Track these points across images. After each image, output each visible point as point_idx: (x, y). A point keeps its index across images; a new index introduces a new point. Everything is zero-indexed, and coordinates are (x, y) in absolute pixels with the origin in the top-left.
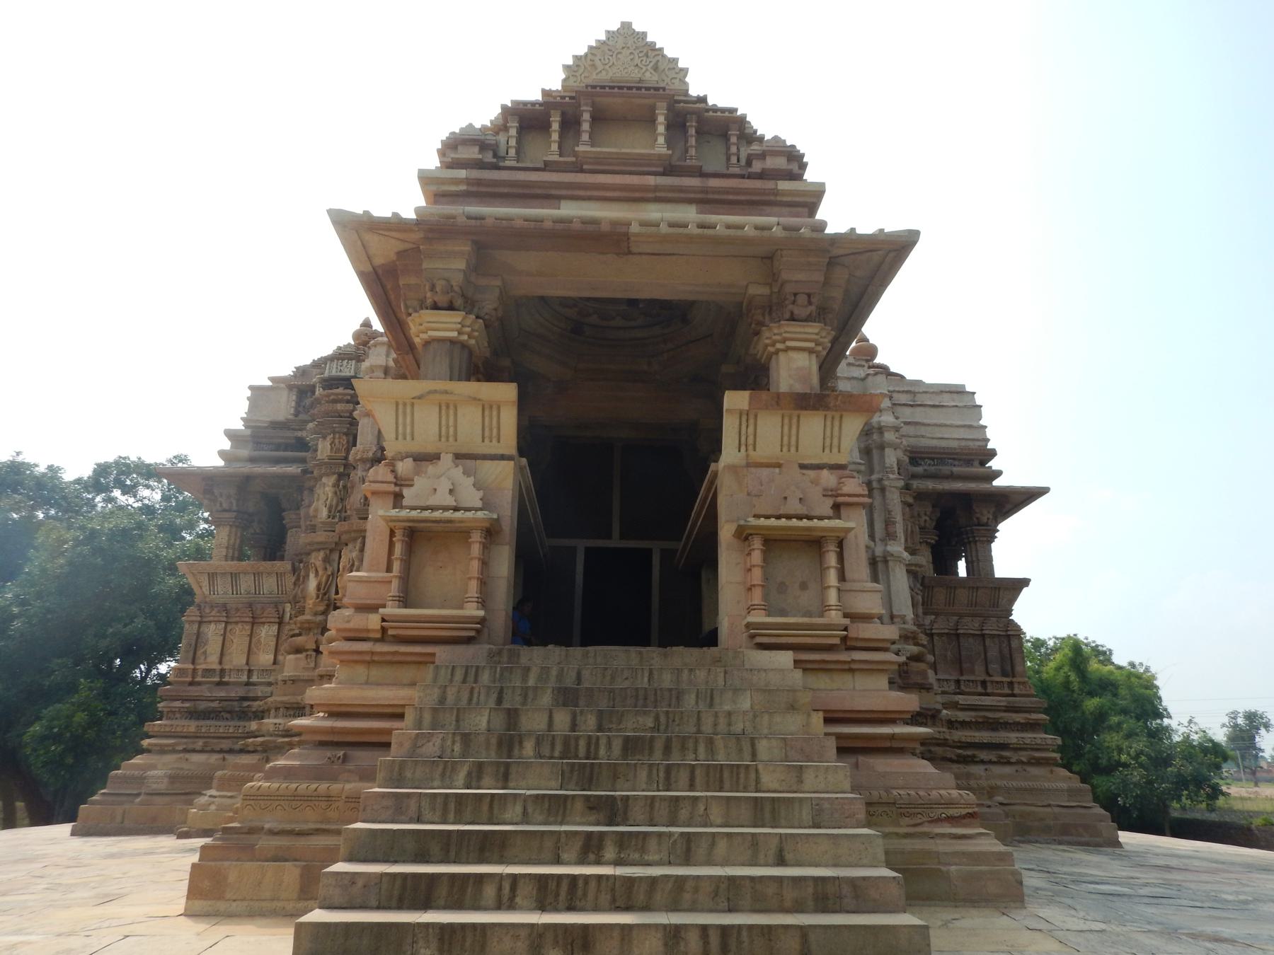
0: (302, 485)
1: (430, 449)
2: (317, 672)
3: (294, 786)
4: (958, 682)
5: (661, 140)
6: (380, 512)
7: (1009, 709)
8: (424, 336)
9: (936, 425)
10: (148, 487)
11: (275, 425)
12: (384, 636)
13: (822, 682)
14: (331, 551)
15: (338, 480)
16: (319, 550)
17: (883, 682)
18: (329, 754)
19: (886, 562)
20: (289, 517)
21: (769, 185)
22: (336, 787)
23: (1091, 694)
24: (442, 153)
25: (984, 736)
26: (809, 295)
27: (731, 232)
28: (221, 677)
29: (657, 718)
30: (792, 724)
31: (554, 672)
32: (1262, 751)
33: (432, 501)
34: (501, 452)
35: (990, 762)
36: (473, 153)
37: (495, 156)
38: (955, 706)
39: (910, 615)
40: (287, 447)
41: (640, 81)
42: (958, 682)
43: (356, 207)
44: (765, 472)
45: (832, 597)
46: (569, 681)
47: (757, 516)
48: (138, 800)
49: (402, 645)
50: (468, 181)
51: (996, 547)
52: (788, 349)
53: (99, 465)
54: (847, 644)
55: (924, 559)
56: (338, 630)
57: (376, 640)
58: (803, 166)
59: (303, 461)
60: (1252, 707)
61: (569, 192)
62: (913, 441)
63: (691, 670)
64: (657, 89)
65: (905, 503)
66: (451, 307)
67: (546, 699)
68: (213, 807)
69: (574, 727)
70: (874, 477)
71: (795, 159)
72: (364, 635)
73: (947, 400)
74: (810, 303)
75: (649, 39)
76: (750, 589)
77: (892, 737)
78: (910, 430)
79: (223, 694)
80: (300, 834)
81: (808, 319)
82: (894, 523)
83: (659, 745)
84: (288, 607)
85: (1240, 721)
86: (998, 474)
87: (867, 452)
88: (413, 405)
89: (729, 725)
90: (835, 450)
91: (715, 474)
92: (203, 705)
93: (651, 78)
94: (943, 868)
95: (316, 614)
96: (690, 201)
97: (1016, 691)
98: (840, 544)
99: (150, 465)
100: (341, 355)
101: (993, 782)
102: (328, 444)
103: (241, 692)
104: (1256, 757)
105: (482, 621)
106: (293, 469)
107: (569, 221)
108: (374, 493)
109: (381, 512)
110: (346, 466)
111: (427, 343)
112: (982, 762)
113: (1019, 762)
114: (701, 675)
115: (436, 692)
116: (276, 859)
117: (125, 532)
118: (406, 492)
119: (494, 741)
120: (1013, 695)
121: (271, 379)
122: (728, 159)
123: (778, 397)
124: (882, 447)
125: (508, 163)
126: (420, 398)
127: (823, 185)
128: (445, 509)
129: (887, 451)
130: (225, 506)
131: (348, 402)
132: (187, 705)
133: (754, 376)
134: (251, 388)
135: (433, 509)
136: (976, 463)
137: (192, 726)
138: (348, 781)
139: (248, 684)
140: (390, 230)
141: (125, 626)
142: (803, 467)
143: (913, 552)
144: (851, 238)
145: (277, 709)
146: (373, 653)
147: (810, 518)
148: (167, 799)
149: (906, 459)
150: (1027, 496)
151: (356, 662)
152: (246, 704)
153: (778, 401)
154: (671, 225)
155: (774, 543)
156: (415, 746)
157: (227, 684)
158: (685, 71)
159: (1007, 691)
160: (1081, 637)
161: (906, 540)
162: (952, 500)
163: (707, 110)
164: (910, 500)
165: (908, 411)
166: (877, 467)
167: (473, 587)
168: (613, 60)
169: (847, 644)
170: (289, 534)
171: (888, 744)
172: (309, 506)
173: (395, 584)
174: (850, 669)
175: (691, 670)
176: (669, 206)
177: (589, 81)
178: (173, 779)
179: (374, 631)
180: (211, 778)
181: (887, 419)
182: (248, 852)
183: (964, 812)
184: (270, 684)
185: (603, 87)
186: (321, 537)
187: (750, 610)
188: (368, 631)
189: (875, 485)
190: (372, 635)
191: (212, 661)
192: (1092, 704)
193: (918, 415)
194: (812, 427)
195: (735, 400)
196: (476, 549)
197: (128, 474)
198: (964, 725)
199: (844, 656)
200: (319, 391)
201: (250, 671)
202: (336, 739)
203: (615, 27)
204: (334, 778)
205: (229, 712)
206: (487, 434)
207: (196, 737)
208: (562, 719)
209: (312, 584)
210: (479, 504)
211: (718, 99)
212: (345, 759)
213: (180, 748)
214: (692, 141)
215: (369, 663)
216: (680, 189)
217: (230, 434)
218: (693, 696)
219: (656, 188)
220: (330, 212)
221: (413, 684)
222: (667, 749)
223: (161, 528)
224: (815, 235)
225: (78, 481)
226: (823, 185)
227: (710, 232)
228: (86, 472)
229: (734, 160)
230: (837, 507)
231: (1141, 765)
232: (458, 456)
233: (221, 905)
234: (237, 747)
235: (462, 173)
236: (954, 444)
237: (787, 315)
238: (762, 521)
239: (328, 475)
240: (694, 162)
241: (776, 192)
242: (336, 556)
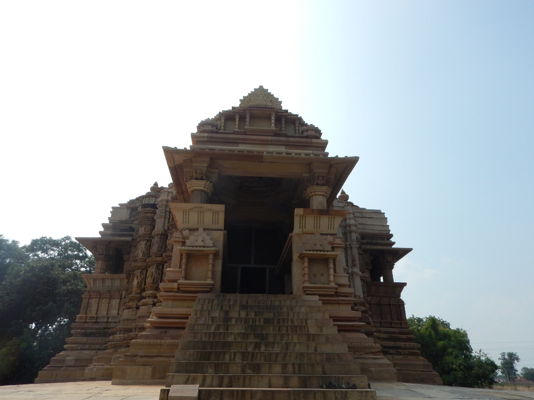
0: (130, 246)
1: (195, 227)
2: (137, 316)
3: (149, 341)
4: (381, 322)
5: (273, 125)
6: (177, 248)
8: (192, 189)
9: (371, 225)
10: (53, 250)
11: (121, 222)
13: (329, 307)
14: (143, 269)
15: (147, 243)
16: (138, 269)
17: (349, 308)
18: (160, 330)
19: (353, 275)
20: (125, 257)
21: (309, 140)
22: (163, 341)
23: (440, 340)
24: (198, 127)
25: (392, 344)
26: (323, 177)
27: (297, 156)
28: (97, 320)
29: (274, 314)
30: (319, 316)
31: (239, 301)
32: (517, 371)
34: (219, 228)
35: (394, 354)
36: (209, 128)
37: (217, 129)
39: (362, 296)
40: (125, 230)
41: (266, 105)
43: (171, 145)
44: (309, 236)
46: (244, 303)
47: (306, 250)
48: (62, 369)
49: (185, 294)
50: (208, 137)
51: (394, 271)
52: (316, 195)
53: (33, 240)
54: (337, 294)
55: (367, 275)
56: (163, 288)
57: (176, 292)
58: (321, 134)
59: (132, 235)
60: (514, 351)
61: (242, 141)
62: (362, 231)
63: (285, 301)
64: (272, 108)
65: (359, 253)
67: (237, 308)
68: (95, 369)
69: (247, 315)
70: (348, 243)
71: (317, 132)
72: (172, 290)
73: (374, 216)
74: (323, 180)
75: (269, 91)
76: (304, 276)
77: (353, 326)
78: (361, 226)
80: (152, 357)
81: (323, 185)
82: (355, 261)
83: (276, 321)
84: (124, 292)
85: (506, 357)
86: (394, 243)
87: (345, 234)
88: (189, 212)
89: (298, 316)
90: (332, 229)
91: (291, 237)
93: (270, 104)
94: (370, 369)
95: (136, 294)
96: (283, 145)
97: (403, 326)
98: (334, 260)
99: (55, 240)
100: (148, 195)
102: (143, 229)
103: (104, 325)
104: (515, 374)
105: (213, 285)
107: (242, 151)
108: (175, 242)
109: (179, 247)
110: (150, 237)
111: (193, 191)
112: (391, 354)
113: (405, 354)
114: (288, 302)
115: (200, 306)
116: (143, 365)
117: (46, 267)
118: (187, 241)
119: (222, 319)
120: (402, 328)
121: (119, 204)
122: (295, 131)
123: (313, 211)
124: (350, 232)
125: (221, 131)
126: (192, 209)
127: (327, 141)
128: (200, 247)
130: (101, 253)
131: (151, 213)
133: (305, 204)
134: (113, 208)
135: (196, 247)
136: (386, 239)
137: (84, 339)
138: (167, 340)
139: (107, 322)
140: (183, 153)
141: (44, 306)
142: (321, 234)
143: (362, 272)
144: (336, 159)
145: (120, 331)
146: (175, 296)
147: (324, 251)
148: (74, 368)
149: (359, 237)
150: (404, 252)
151: (168, 299)
152: (106, 330)
153: (313, 212)
154: (277, 153)
155: (313, 260)
156: (196, 321)
157: (99, 322)
158: (281, 102)
159: (399, 326)
160: (436, 317)
161: (360, 268)
162: (377, 251)
163: (288, 115)
164: (361, 252)
165: (360, 219)
166: (349, 240)
167: (210, 274)
168: (257, 98)
169: (337, 294)
170: (125, 263)
171: (351, 328)
172: (134, 253)
173: (183, 272)
174: (338, 303)
175: (285, 301)
176: (276, 147)
177: (249, 105)
178: (76, 360)
179: (175, 288)
180: (92, 360)
181: (352, 222)
183: (377, 350)
184: (116, 322)
185: (254, 107)
186: (139, 264)
188: (173, 288)
189: (348, 246)
190: (174, 290)
191: (93, 314)
192: (440, 344)
193: (364, 221)
194: (324, 221)
195: (298, 211)
196: (211, 261)
197: (44, 244)
199: (336, 299)
200: (140, 209)
201: (108, 318)
202: (162, 325)
203: (257, 87)
204: (162, 339)
205: (99, 334)
206: (214, 222)
207: (85, 344)
208: (243, 314)
209: (135, 282)
210: (212, 245)
211: (293, 110)
212: (166, 332)
213: (79, 348)
214: (283, 125)
215: (173, 300)
216: (280, 141)
217: (104, 225)
218: (286, 308)
219: (271, 141)
220: (163, 147)
221: (188, 307)
222: (278, 322)
223: (59, 266)
224: (325, 157)
225: (24, 247)
226: (327, 141)
227: (290, 156)
228: (28, 243)
229: (297, 131)
230: (333, 248)
231: (461, 370)
232: (204, 229)
233: (125, 381)
234: (102, 348)
235: (206, 135)
236: (377, 232)
237: (316, 183)
238: (308, 252)
239: (143, 240)
240: (284, 132)
241: (312, 143)
242: (145, 272)
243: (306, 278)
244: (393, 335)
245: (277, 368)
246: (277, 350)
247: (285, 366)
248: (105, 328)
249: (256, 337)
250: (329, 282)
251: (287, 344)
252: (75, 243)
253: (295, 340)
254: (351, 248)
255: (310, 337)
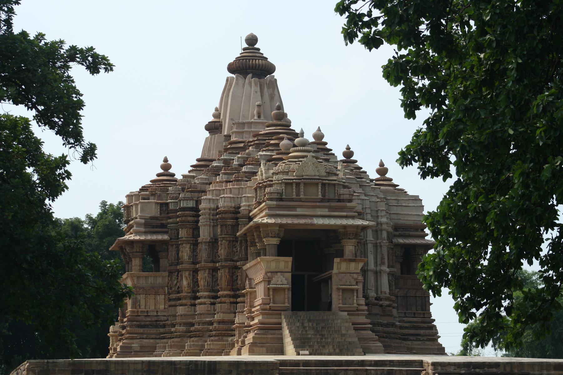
4: (405, 313)
7: (422, 322)
11: (152, 218)
12: (270, 309)
13: (353, 317)
17: (364, 317)
19: (381, 273)
25: (412, 332)
28: (157, 313)
30: (347, 325)
33: (278, 283)
35: (414, 340)
38: (403, 321)
42: (405, 313)
44: (342, 275)
45: (355, 301)
54: (358, 310)
55: (397, 270)
62: (396, 221)
66: (274, 237)
70: (378, 241)
79: (150, 319)
92: (143, 323)
97: (426, 316)
101: (413, 346)
103: (156, 318)
106: (166, 237)
112: (411, 340)
113: (423, 340)
114: (331, 317)
124: (381, 230)
129: (383, 232)
132: (138, 323)
133: (340, 254)
153: (345, 260)
155: (344, 290)
157: (149, 316)
165: (395, 208)
166: (379, 238)
169: (358, 310)
174: (358, 315)
180: (156, 347)
181: (384, 220)
182: (257, 346)
187: (339, 304)
189: (378, 244)
194: (353, 265)
195: (336, 260)
198: (406, 328)
208: (310, 324)
214: (327, 188)
236: (411, 223)
243: (341, 302)
244: (415, 324)
245: (331, 347)
246: (329, 340)
247: (333, 346)
248: (156, 321)
249: (320, 335)
250: (353, 304)
251: (333, 338)
252: (285, 318)
253: (336, 336)
254: (381, 246)
255: (343, 335)
